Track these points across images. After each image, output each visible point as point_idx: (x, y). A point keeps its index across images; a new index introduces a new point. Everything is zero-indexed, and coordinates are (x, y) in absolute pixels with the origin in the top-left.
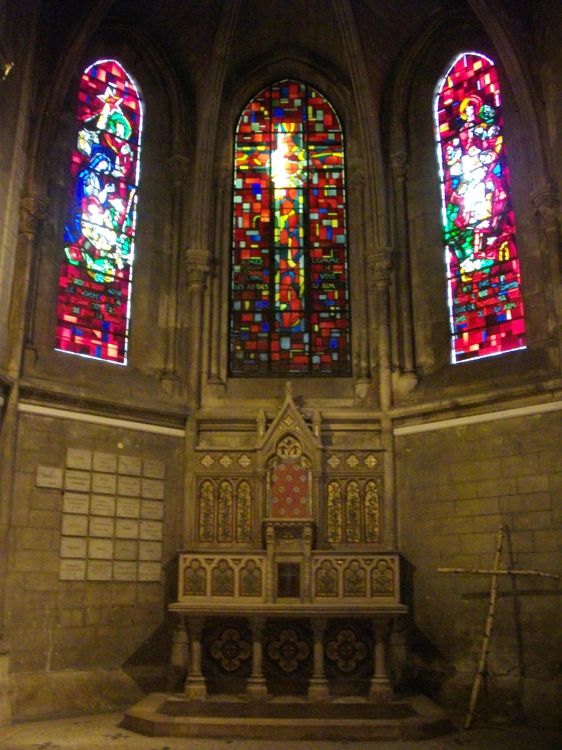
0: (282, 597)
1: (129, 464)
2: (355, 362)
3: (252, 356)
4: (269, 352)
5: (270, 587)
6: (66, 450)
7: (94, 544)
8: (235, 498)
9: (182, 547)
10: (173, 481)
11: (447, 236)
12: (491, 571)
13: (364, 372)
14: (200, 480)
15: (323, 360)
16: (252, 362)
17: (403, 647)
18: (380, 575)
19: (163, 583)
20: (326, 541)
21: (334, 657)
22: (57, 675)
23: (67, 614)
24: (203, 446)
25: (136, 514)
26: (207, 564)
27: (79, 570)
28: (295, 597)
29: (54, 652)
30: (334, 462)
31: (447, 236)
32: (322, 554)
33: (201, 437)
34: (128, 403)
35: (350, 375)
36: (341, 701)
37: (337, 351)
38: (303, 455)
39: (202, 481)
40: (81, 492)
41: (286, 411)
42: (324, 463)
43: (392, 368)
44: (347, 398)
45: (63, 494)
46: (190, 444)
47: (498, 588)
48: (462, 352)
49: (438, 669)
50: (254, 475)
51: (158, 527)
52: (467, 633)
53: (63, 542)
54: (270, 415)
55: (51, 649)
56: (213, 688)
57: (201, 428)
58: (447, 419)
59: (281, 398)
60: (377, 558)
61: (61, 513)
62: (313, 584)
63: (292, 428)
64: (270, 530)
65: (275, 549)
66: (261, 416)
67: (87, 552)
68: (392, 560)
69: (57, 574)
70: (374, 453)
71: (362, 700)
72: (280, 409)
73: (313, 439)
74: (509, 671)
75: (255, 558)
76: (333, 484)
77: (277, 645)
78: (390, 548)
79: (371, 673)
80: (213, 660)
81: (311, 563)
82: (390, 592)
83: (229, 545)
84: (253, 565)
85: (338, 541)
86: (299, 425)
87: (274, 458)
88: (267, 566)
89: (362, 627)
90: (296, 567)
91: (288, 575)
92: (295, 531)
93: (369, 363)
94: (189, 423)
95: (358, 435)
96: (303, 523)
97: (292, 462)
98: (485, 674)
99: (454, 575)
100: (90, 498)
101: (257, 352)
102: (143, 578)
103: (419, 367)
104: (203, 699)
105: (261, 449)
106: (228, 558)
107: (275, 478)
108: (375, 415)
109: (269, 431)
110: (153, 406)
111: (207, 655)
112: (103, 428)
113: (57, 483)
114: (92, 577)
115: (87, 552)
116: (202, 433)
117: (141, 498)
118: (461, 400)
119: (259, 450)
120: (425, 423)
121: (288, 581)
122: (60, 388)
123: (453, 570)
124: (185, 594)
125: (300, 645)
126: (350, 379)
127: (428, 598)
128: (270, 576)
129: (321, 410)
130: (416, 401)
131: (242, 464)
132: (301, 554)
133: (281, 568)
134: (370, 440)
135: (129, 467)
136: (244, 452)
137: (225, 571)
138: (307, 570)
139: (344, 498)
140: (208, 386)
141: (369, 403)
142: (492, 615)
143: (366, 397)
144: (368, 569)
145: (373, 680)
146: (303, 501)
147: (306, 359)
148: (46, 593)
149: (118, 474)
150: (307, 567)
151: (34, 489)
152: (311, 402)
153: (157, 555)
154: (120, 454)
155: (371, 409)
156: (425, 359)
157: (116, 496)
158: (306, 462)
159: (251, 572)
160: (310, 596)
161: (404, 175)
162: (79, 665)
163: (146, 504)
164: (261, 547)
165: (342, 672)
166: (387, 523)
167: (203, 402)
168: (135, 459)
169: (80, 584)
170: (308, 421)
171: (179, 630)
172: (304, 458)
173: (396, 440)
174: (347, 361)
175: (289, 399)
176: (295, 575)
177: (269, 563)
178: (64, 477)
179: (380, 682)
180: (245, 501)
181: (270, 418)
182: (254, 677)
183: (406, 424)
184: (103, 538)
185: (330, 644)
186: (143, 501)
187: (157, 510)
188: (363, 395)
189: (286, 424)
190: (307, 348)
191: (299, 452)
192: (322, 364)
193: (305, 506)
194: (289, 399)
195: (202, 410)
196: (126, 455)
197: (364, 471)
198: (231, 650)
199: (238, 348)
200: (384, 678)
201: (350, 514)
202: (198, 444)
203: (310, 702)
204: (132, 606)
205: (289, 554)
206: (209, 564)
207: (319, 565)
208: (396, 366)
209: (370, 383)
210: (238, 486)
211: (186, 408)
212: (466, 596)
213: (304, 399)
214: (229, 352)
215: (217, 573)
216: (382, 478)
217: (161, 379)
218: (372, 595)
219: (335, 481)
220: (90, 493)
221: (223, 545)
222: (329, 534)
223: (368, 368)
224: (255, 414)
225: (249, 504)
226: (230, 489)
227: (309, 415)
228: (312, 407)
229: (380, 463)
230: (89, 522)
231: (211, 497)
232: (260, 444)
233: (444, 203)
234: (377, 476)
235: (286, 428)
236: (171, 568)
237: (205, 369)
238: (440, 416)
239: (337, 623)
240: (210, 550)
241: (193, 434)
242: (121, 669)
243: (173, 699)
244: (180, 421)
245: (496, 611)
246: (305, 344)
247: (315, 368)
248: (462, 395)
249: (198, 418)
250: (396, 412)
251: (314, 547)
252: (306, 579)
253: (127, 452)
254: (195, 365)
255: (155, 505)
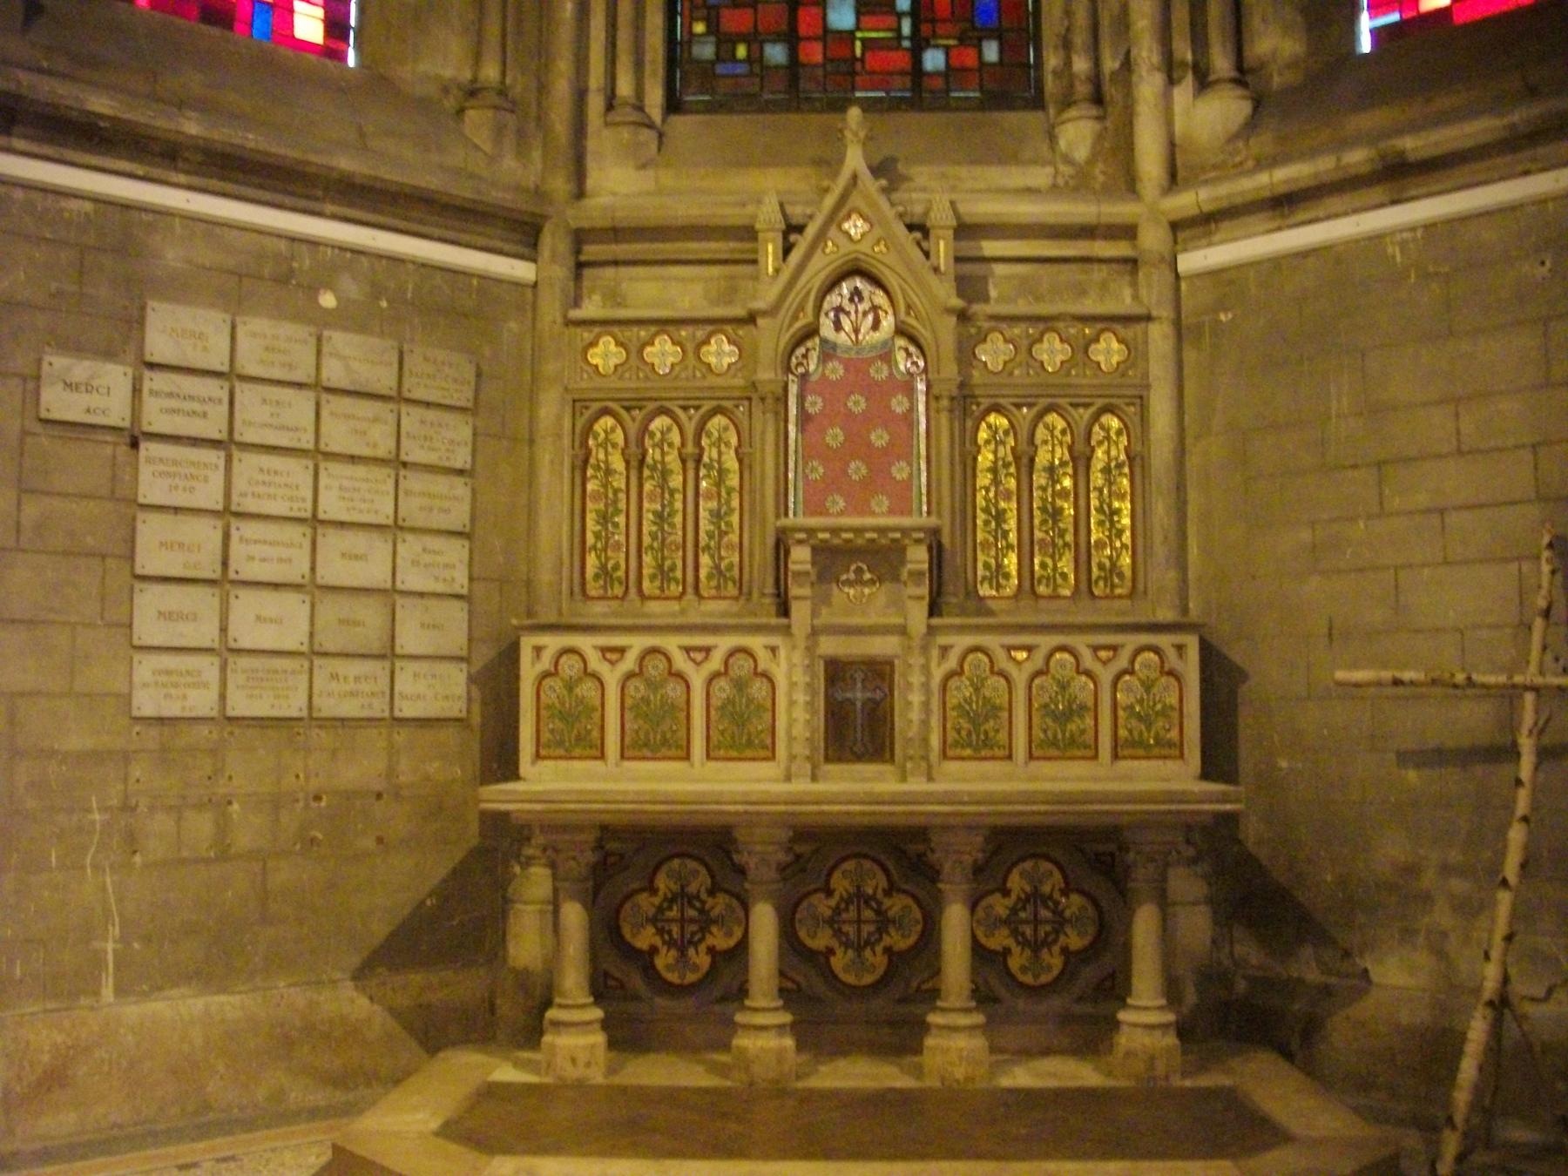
0: (840, 760)
1: (355, 357)
2: (1052, 61)
3: (741, 51)
4: (792, 39)
5: (800, 731)
6: (143, 308)
7: (246, 605)
8: (691, 465)
9: (530, 613)
10: (497, 414)
12: (1518, 679)
13: (1083, 89)
14: (586, 408)
15: (955, 63)
16: (742, 69)
17: (1203, 908)
18: (1140, 692)
19: (476, 719)
20: (971, 593)
21: (998, 940)
22: (133, 1011)
23: (162, 823)
24: (592, 308)
25: (383, 511)
26: (607, 665)
27: (196, 685)
28: (884, 762)
29: (124, 939)
30: (993, 353)
32: (961, 629)
33: (586, 283)
34: (345, 163)
35: (1037, 102)
36: (1022, 1077)
37: (999, 35)
38: (900, 331)
39: (587, 414)
40: (195, 442)
41: (844, 198)
42: (966, 354)
43: (1171, 71)
44: (1034, 162)
45: (134, 444)
46: (550, 309)
47: (1541, 732)
48: (1394, 17)
49: (1313, 976)
50: (751, 394)
51: (456, 552)
52: (1411, 870)
53: (139, 599)
54: (797, 212)
55: (115, 931)
56: (626, 1036)
57: (583, 258)
58: (1356, 211)
59: (829, 163)
60: (1132, 641)
61: (131, 507)
62: (935, 722)
63: (864, 247)
64: (800, 556)
65: (815, 613)
66: (768, 216)
67: (224, 630)
68: (1180, 648)
69: (127, 699)
70: (1118, 327)
71: (1081, 1074)
72: (827, 190)
73: (933, 280)
74: (1550, 991)
75: (756, 642)
76: (992, 418)
77: (823, 906)
78: (1166, 615)
79: (1115, 988)
80: (630, 953)
81: (928, 660)
82: (1170, 744)
83: (675, 606)
84: (747, 664)
85: (1008, 592)
86: (888, 239)
87: (809, 344)
88: (791, 666)
89: (1093, 855)
90: (879, 672)
91: (859, 695)
92: (882, 558)
93: (1097, 62)
94: (546, 240)
95: (1067, 273)
96: (905, 531)
97: (866, 355)
98: (1501, 1004)
99: (1391, 691)
100: (229, 460)
101: (755, 40)
102: (407, 710)
103: (1252, 71)
104: (597, 1077)
105: (772, 312)
106: (671, 643)
107: (815, 404)
108: (1119, 211)
109: (795, 256)
110: (431, 181)
111: (608, 934)
112: (269, 243)
113: (116, 411)
114: (239, 705)
115: (224, 630)
116: (587, 272)
117: (398, 463)
118: (1413, 145)
119: (765, 313)
120: (1279, 229)
121: (857, 718)
122: (105, 101)
123: (1387, 675)
124: (538, 756)
125: (896, 905)
126: (1040, 114)
127: (1284, 764)
128: (801, 697)
129: (954, 197)
130: (1250, 163)
131: (713, 360)
132: (902, 631)
133: (836, 671)
134: (1104, 286)
135: (355, 365)
136: (717, 323)
137: (662, 684)
138: (916, 679)
139: (1025, 461)
140: (606, 133)
141: (1101, 178)
142: (1525, 819)
143: (1092, 161)
144: (1106, 676)
145: (1122, 1016)
146: (900, 472)
147: (901, 60)
148: (97, 757)
149: (320, 388)
150: (917, 670)
151: (38, 428)
152: (921, 175)
153: (456, 640)
154: (327, 325)
155: (1107, 192)
157: (318, 455)
158: (909, 355)
159: (740, 685)
160: (925, 758)
162: (207, 976)
163: (412, 481)
164: (773, 609)
165: (1021, 985)
166: (1158, 538)
167: (590, 183)
168: (375, 341)
169: (204, 730)
170: (920, 228)
171: (527, 863)
172: (901, 342)
173: (1184, 286)
174: (1028, 65)
175: (855, 159)
176: (878, 695)
177: (798, 657)
178: (136, 391)
179: (1145, 1020)
180: (722, 472)
181: (794, 222)
182: (756, 1010)
183: (1216, 238)
184: (276, 586)
185: (990, 900)
186: (402, 472)
187: (452, 502)
188: (1081, 154)
189: (847, 234)
190: (906, 27)
191: (888, 323)
192: (951, 72)
193: (907, 485)
194: (855, 159)
195: (588, 202)
196: (346, 329)
197: (1082, 378)
198: (682, 921)
199: (699, 28)
200: (1160, 1008)
201: (1043, 509)
202: (577, 303)
203: (931, 1082)
204: (379, 796)
205: (859, 631)
206: (612, 663)
207: (952, 662)
208: (1183, 64)
209: (1099, 118)
210: (701, 429)
211: (539, 194)
212: (1405, 758)
213: (900, 167)
214: (671, 41)
215: (637, 689)
216: (1142, 402)
217: (461, 111)
218: (1116, 756)
219: (997, 409)
220: (226, 444)
221: (654, 607)
222: (980, 572)
223: (1096, 80)
224: (750, 209)
225: (733, 481)
226: (675, 437)
227: (918, 209)
228: (924, 190)
229: (1136, 353)
230: (226, 537)
231: (618, 463)
232: (766, 296)
234: (1126, 397)
235: (846, 247)
236: (497, 682)
237: (596, 79)
238: (1334, 203)
239: (1010, 841)
240: (613, 621)
241: (560, 272)
242: (350, 984)
243: (506, 1073)
244: (523, 233)
245: (1535, 806)
246: (900, 15)
247: (926, 82)
248: (1414, 128)
249: (573, 224)
250: (1186, 202)
251: (934, 610)
252: (913, 708)
253: (345, 319)
254: (563, 66)
255: (441, 484)
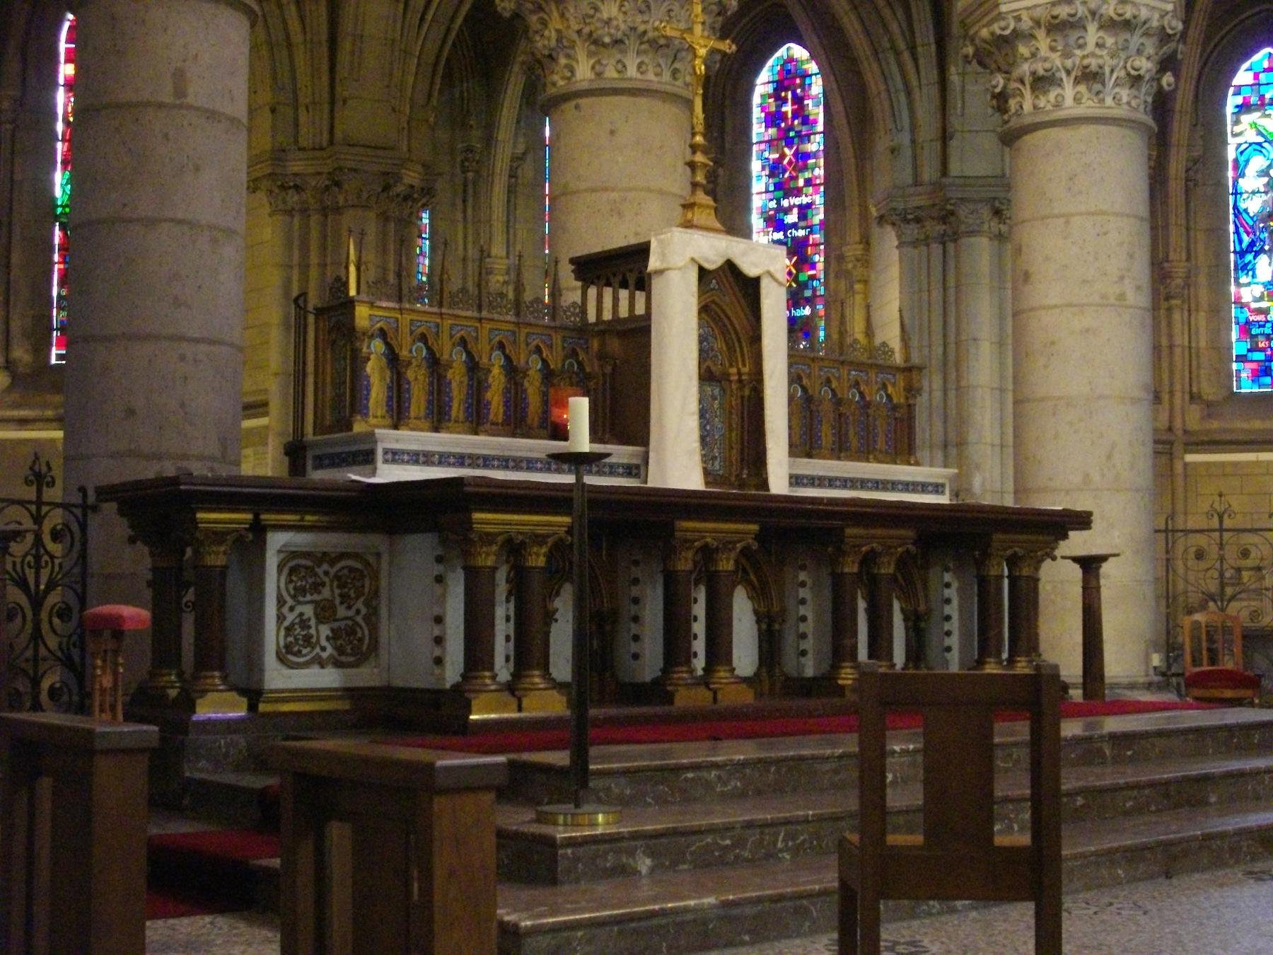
11: (59, 210)
31: (59, 210)
65: (1189, 151)
156: (21, 354)
161: (13, 122)
233: (59, 165)
